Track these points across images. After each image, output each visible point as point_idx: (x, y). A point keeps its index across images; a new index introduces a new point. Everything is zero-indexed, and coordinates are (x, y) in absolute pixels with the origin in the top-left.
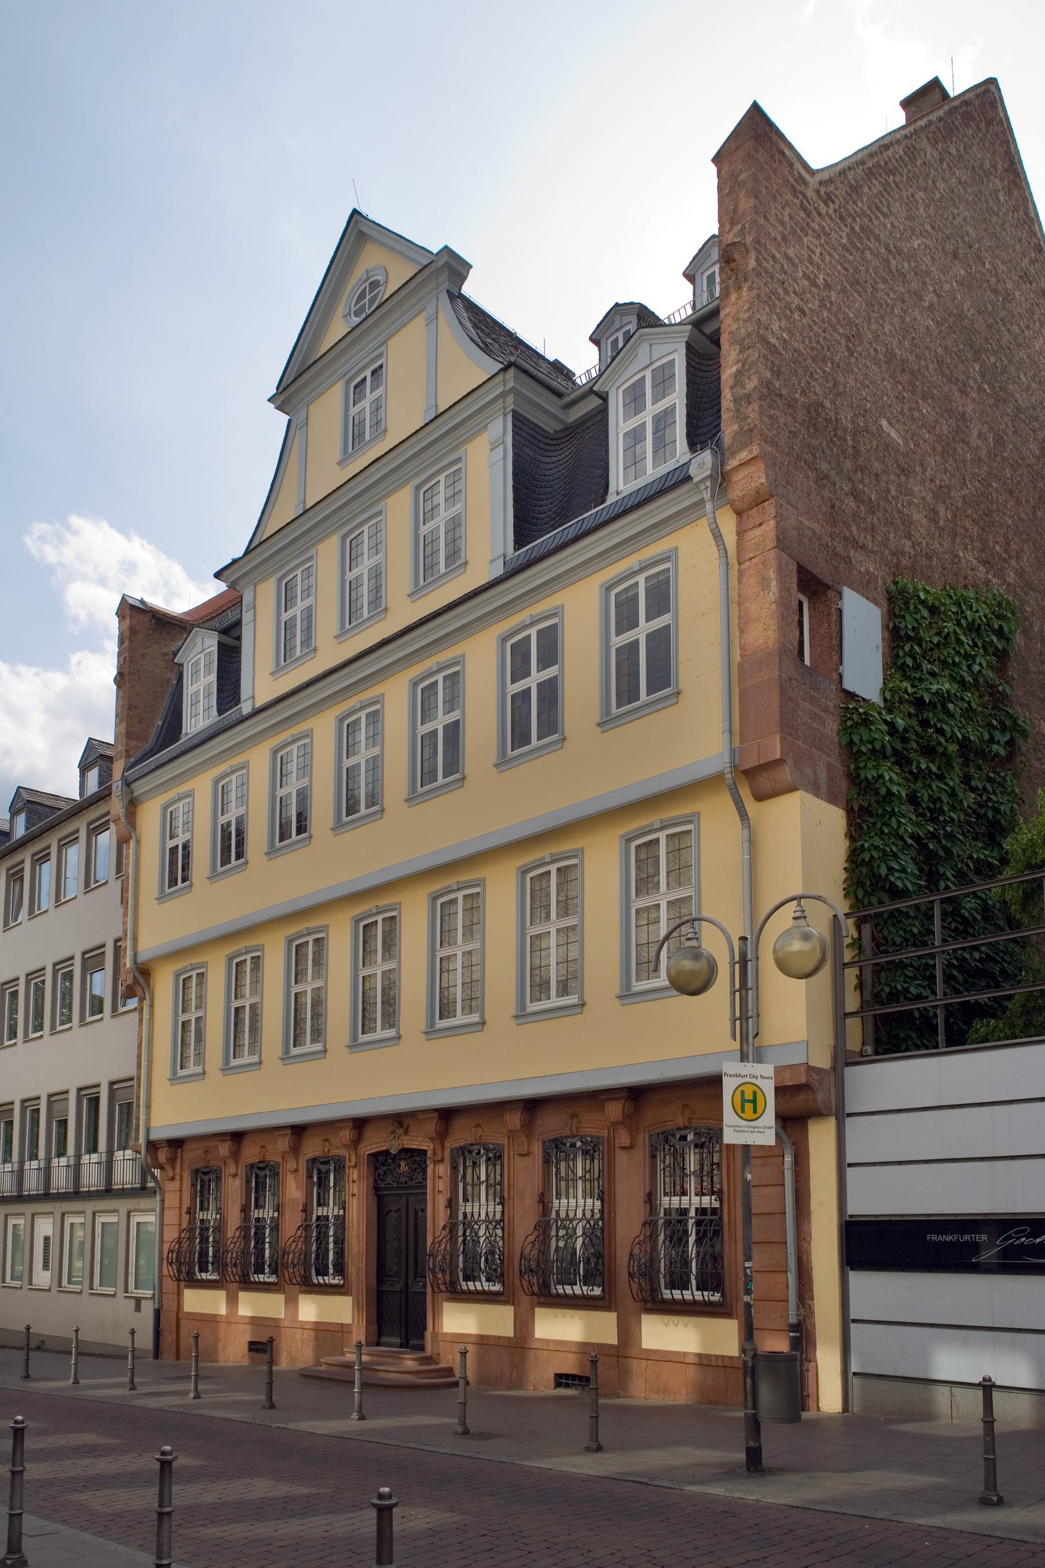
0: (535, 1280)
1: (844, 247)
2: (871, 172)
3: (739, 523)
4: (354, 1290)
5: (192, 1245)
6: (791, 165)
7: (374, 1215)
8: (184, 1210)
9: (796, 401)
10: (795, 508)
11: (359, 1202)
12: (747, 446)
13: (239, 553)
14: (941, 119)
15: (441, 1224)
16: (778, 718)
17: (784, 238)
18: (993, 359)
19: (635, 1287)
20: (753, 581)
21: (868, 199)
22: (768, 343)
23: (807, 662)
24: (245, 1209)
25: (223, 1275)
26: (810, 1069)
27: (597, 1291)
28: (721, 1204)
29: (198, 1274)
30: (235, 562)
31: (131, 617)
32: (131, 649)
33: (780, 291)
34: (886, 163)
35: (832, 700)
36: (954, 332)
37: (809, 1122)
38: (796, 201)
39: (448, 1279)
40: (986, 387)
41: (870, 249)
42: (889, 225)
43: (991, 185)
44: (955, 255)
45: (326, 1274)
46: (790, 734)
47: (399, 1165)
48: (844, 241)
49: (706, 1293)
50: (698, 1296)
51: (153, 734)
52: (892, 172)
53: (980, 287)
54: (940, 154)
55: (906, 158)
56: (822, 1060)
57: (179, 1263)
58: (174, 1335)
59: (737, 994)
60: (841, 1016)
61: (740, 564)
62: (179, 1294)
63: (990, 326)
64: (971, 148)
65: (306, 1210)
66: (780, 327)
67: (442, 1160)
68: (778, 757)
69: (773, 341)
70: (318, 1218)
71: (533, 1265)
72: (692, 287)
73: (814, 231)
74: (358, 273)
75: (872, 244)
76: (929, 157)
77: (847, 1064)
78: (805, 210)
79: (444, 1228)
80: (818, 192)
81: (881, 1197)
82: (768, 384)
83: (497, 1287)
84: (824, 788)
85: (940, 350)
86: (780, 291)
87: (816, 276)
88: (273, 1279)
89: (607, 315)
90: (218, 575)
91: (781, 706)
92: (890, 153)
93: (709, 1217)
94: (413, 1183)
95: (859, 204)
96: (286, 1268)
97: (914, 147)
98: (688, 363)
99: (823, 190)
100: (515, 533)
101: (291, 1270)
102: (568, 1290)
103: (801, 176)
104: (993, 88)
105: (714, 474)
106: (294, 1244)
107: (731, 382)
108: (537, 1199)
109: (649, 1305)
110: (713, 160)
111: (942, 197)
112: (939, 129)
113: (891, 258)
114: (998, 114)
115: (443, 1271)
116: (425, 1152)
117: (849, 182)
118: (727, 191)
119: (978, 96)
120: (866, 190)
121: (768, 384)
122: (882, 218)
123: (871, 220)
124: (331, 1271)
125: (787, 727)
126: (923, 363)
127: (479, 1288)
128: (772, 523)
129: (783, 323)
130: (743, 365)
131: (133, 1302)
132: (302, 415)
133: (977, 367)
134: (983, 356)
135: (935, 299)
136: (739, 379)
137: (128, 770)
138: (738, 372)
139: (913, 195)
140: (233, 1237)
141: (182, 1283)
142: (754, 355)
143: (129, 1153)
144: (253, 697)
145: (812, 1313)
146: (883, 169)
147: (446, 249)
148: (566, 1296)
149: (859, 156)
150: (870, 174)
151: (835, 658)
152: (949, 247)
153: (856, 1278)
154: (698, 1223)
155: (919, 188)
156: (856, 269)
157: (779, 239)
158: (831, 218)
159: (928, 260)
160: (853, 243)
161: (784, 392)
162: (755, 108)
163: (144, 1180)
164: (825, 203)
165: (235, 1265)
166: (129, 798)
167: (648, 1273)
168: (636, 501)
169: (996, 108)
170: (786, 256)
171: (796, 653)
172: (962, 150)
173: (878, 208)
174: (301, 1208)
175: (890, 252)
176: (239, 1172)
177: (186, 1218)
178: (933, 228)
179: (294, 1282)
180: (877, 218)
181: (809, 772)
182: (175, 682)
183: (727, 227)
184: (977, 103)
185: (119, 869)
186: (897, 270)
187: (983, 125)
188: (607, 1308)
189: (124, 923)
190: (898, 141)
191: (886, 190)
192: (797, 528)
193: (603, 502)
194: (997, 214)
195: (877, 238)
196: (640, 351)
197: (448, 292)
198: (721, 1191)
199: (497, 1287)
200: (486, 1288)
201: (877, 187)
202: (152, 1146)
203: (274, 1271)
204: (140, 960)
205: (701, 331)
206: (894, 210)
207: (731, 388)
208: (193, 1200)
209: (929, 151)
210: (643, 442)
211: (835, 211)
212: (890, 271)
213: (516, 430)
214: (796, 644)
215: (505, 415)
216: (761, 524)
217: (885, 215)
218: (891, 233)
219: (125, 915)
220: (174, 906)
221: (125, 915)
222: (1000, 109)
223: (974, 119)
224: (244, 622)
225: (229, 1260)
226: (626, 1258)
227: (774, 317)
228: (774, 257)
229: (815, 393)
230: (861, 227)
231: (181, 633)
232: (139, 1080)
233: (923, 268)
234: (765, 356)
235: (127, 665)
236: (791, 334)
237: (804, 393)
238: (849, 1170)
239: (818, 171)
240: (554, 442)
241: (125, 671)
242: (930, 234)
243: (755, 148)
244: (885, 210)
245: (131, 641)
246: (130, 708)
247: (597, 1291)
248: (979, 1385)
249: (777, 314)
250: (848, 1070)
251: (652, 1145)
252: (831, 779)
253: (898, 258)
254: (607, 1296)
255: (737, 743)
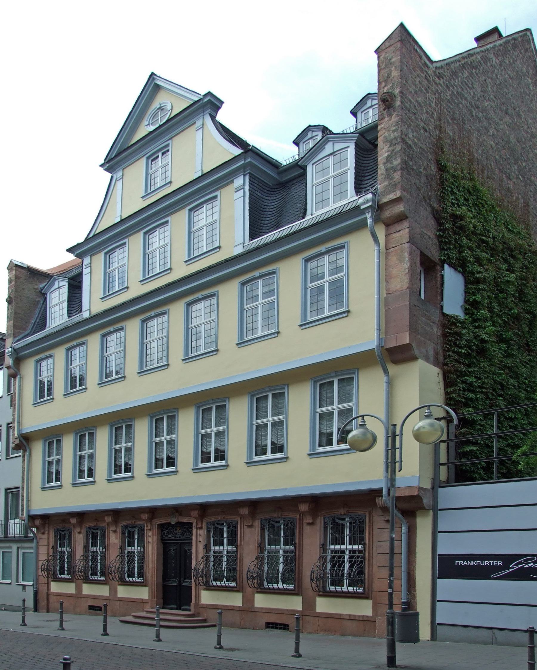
0: (256, 581)
1: (448, 101)
2: (463, 66)
3: (387, 230)
4: (150, 583)
5: (55, 563)
6: (421, 57)
7: (161, 552)
8: (51, 547)
9: (421, 173)
10: (419, 224)
11: (152, 545)
12: (394, 191)
13: (82, 240)
14: (501, 45)
15: (201, 556)
16: (408, 324)
17: (416, 92)
18: (524, 164)
19: (314, 585)
20: (394, 258)
21: (461, 79)
22: (406, 143)
23: (423, 297)
24: (86, 548)
25: (74, 576)
26: (420, 488)
27: (291, 587)
28: (365, 548)
29: (90, 576)
30: (78, 244)
31: (16, 270)
32: (16, 286)
33: (413, 118)
34: (471, 62)
35: (436, 317)
36: (504, 149)
37: (418, 513)
38: (422, 75)
39: (205, 580)
40: (520, 177)
41: (462, 104)
42: (472, 93)
43: (526, 81)
44: (506, 113)
45: (96, 575)
46: (415, 332)
47: (176, 529)
48: (449, 98)
49: (355, 588)
50: (227, 584)
51: (30, 326)
52: (475, 68)
53: (519, 129)
54: (500, 62)
55: (482, 62)
56: (427, 485)
57: (48, 571)
58: (46, 602)
59: (390, 451)
60: (437, 465)
61: (387, 250)
62: (48, 584)
63: (523, 148)
64: (516, 61)
65: (122, 548)
66: (413, 136)
67: (201, 528)
68: (408, 342)
69: (410, 142)
70: (129, 552)
71: (255, 575)
72: (355, 119)
73: (432, 91)
74: (155, 105)
75: (464, 102)
76: (494, 63)
77: (440, 487)
78: (428, 80)
79: (202, 558)
80: (435, 72)
81: (448, 547)
82: (406, 163)
83: (233, 584)
84: (431, 358)
85: (497, 157)
86: (413, 118)
87: (433, 113)
88: (69, 577)
89: (304, 131)
90: (69, 250)
91: (410, 318)
92: (473, 58)
93: (357, 554)
94: (184, 538)
95: (457, 81)
96: (111, 574)
97: (486, 56)
98: (356, 153)
99: (437, 71)
100: (250, 233)
101: (113, 575)
102: (218, 583)
103: (425, 64)
104: (528, 33)
105: (373, 205)
106: (115, 563)
107: (385, 161)
108: (257, 545)
109: (259, 590)
110: (375, 51)
111: (501, 83)
112: (500, 50)
113: (473, 110)
114: (531, 47)
115: (202, 576)
116: (192, 524)
117: (452, 69)
118: (383, 66)
119: (521, 36)
120: (460, 74)
121: (406, 163)
122: (468, 89)
123: (463, 90)
124: (136, 575)
125: (413, 329)
126: (489, 162)
127: (223, 584)
128: (407, 230)
129: (415, 134)
130: (392, 153)
131: (21, 587)
132: (120, 174)
133: (516, 167)
134: (519, 162)
135: (495, 133)
136: (388, 159)
137: (15, 343)
138: (389, 156)
139: (485, 81)
140: (80, 560)
141: (50, 579)
142: (398, 148)
143: (17, 521)
144: (90, 310)
145: (415, 597)
146: (470, 65)
147: (209, 94)
148: (218, 586)
149: (457, 57)
150: (463, 67)
151: (439, 298)
152: (503, 108)
153: (439, 582)
154: (351, 557)
155: (489, 78)
156: (454, 113)
157: (413, 92)
158: (442, 86)
159: (492, 113)
160: (453, 100)
161: (415, 168)
162: (402, 25)
163: (26, 533)
164: (439, 78)
165: (81, 572)
166: (16, 356)
167: (85, 570)
168: (325, 218)
169: (530, 44)
170: (417, 101)
171: (418, 294)
172: (511, 61)
173: (466, 84)
174: (119, 547)
175: (472, 106)
176: (82, 531)
177: (51, 551)
178: (495, 97)
179: (115, 580)
180: (466, 89)
181: (424, 351)
182: (42, 302)
183: (383, 84)
184: (520, 40)
185: (9, 390)
186: (476, 116)
187: (523, 51)
188: (297, 594)
189: (14, 415)
190: (478, 53)
191: (471, 76)
192: (420, 234)
193: (303, 218)
194: (529, 95)
195: (466, 99)
196: (327, 146)
197: (210, 114)
198: (295, 543)
199: (233, 584)
200: (227, 585)
201: (466, 74)
202: (32, 518)
203: (102, 574)
204: (24, 432)
205: (364, 137)
206: (475, 86)
207: (384, 164)
208: (56, 542)
209: (494, 60)
210: (330, 189)
211: (444, 82)
212: (472, 116)
213: (251, 182)
214: (418, 290)
215: (245, 175)
216: (400, 231)
217: (471, 89)
218: (473, 97)
219: (14, 411)
220: (43, 408)
221: (14, 411)
222: (532, 44)
223: (519, 47)
224: (84, 273)
225: (77, 570)
226: (246, 571)
227: (410, 130)
228: (410, 101)
229: (431, 170)
230: (458, 92)
231: (46, 279)
232: (23, 488)
233: (489, 116)
234: (405, 149)
235: (14, 293)
236: (419, 139)
237: (425, 169)
238: (439, 534)
239: (435, 62)
240: (273, 190)
241: (13, 296)
242: (493, 101)
243: (401, 44)
244: (471, 86)
245: (15, 282)
246: (15, 313)
247: (291, 587)
248: (527, 631)
249: (412, 129)
250: (441, 490)
251: (325, 522)
252: (436, 354)
253: (476, 110)
254: (297, 589)
255: (383, 336)
